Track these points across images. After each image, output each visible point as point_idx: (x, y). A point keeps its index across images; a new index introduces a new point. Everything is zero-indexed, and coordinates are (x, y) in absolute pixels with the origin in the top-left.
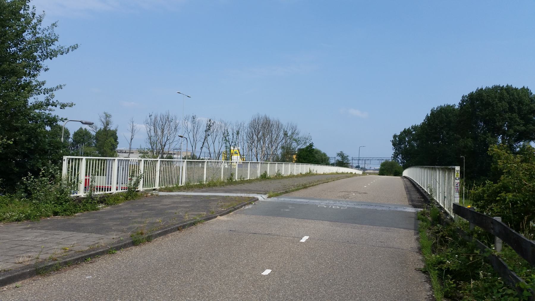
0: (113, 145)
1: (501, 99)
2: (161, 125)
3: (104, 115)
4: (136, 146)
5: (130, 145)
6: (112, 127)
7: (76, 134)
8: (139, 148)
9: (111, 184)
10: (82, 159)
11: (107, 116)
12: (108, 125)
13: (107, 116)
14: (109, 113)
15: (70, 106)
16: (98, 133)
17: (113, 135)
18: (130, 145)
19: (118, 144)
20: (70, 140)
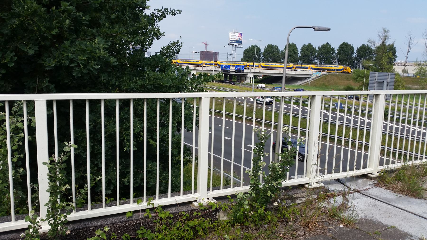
0: (390, 59)
1: (104, 91)
2: (165, 17)
3: (382, 30)
4: (412, 58)
5: (407, 58)
6: (389, 42)
7: (358, 50)
8: (415, 60)
9: (370, 116)
10: (313, 97)
11: (385, 31)
12: (385, 39)
13: (385, 31)
14: (387, 28)
15: (174, 14)
16: (378, 48)
17: (392, 50)
18: (407, 58)
19: (396, 57)
20: (355, 55)
